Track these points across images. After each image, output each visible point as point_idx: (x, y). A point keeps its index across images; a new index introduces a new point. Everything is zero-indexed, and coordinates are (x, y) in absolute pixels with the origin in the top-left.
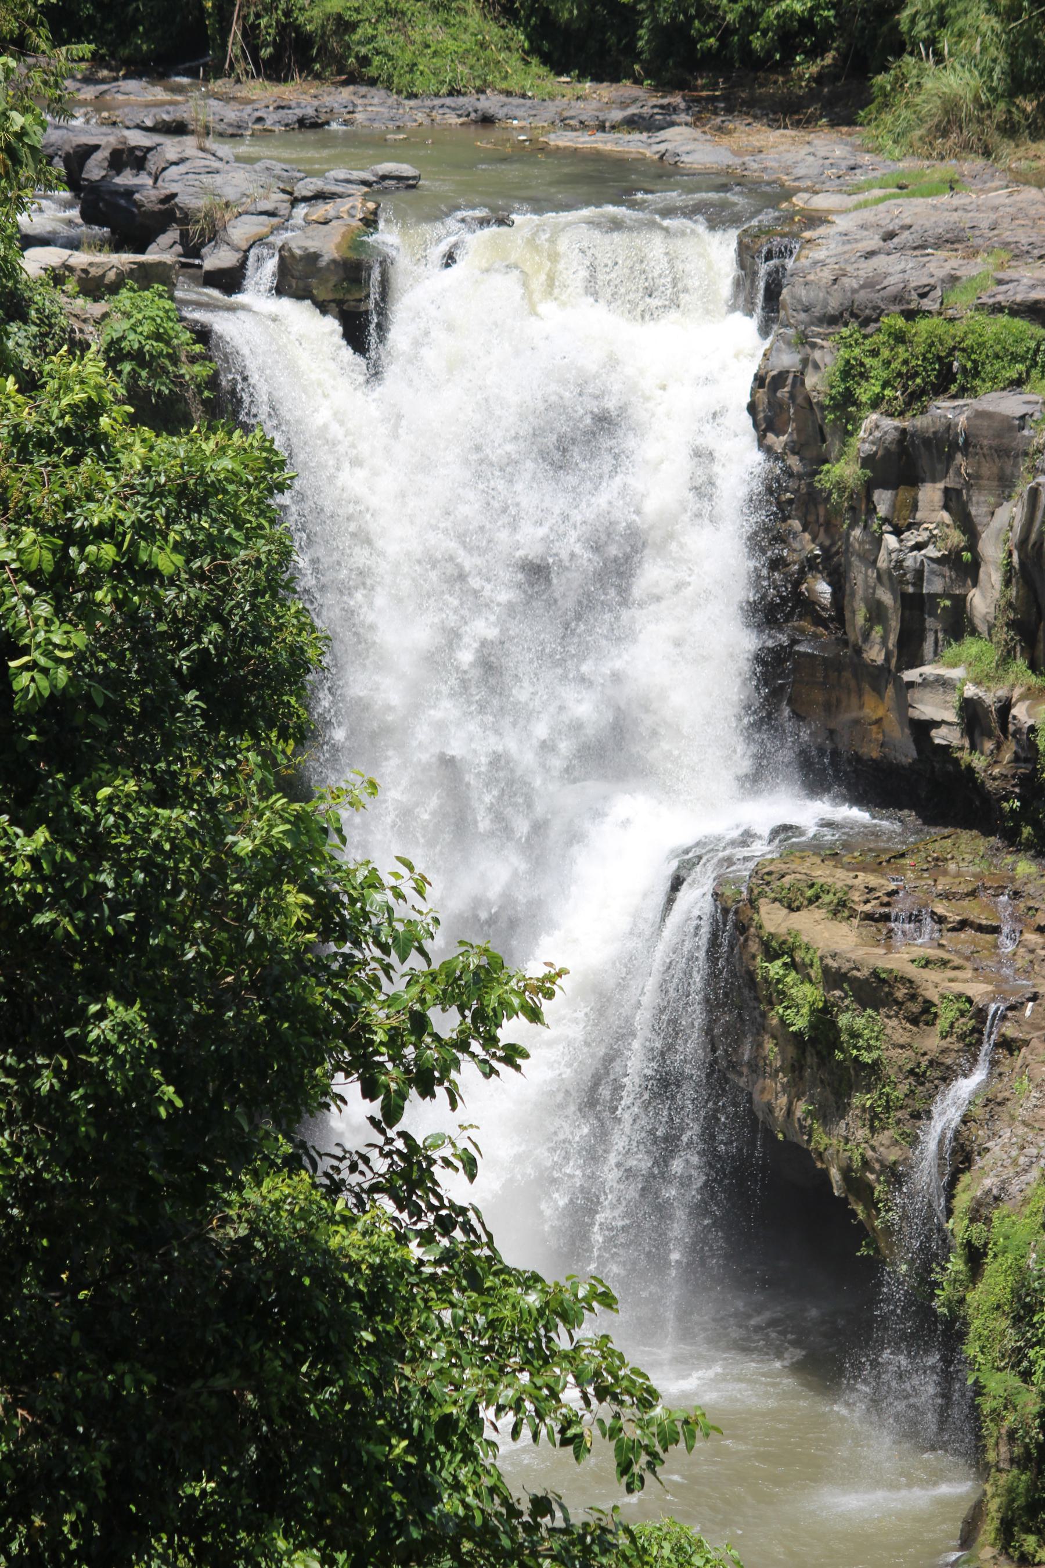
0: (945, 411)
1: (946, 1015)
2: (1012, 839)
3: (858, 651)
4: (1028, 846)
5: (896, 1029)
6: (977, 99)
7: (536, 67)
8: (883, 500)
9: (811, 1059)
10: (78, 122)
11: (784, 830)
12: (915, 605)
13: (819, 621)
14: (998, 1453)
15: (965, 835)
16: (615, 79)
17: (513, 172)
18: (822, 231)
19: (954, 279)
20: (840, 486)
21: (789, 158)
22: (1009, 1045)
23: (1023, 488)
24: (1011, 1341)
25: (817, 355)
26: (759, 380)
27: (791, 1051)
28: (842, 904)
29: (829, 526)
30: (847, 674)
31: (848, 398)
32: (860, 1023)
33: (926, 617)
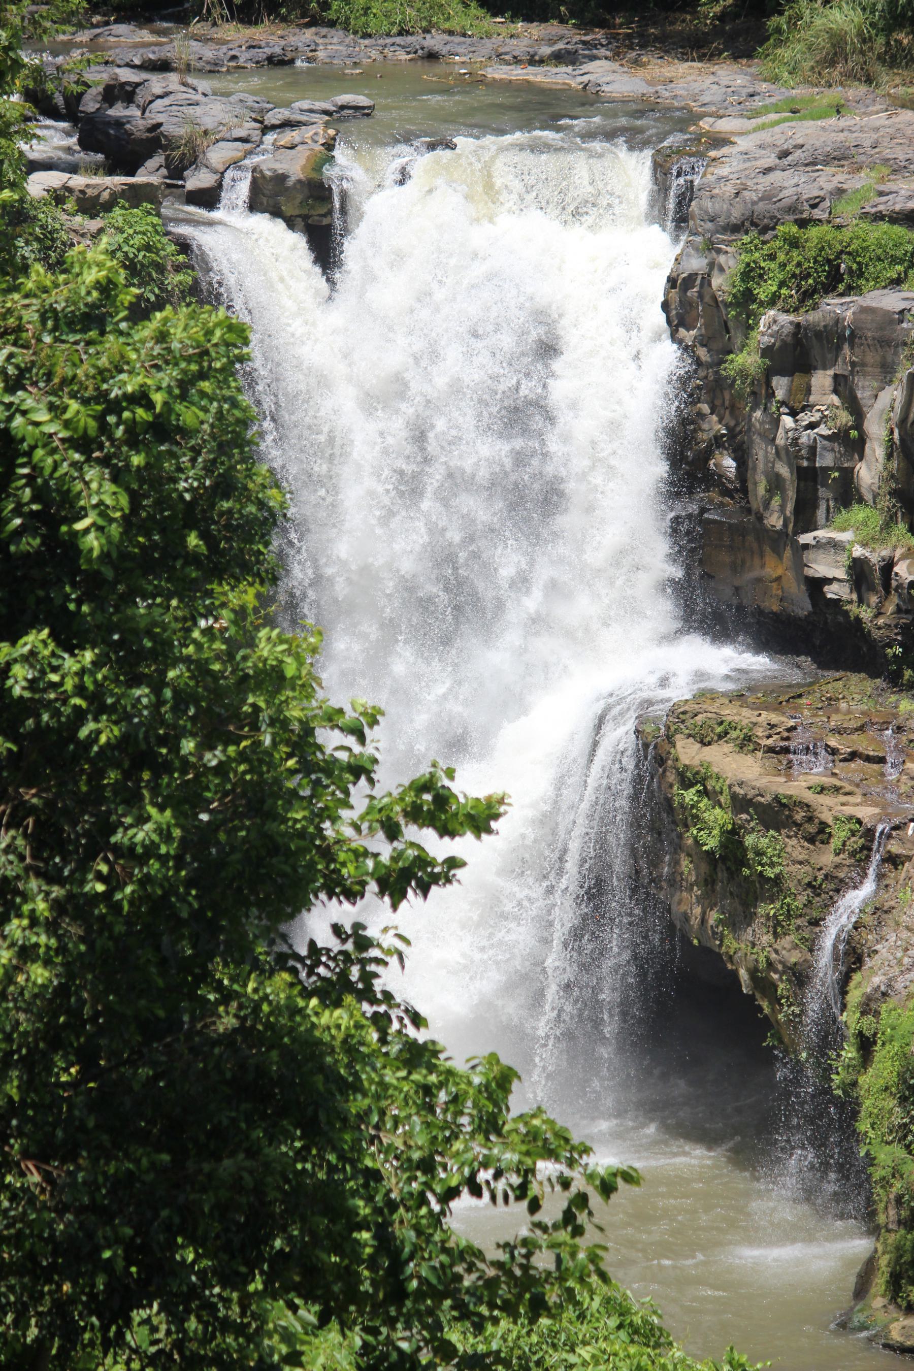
0: (836, 307)
1: (839, 835)
3: (760, 518)
5: (795, 847)
6: (860, 34)
8: (781, 386)
9: (722, 875)
15: (855, 678)
18: (725, 150)
19: (840, 192)
20: (743, 373)
21: (696, 87)
22: (894, 861)
25: (722, 259)
26: (672, 282)
27: (704, 868)
28: (748, 739)
29: (733, 409)
30: (750, 538)
31: (748, 297)
32: (764, 842)
33: (819, 487)
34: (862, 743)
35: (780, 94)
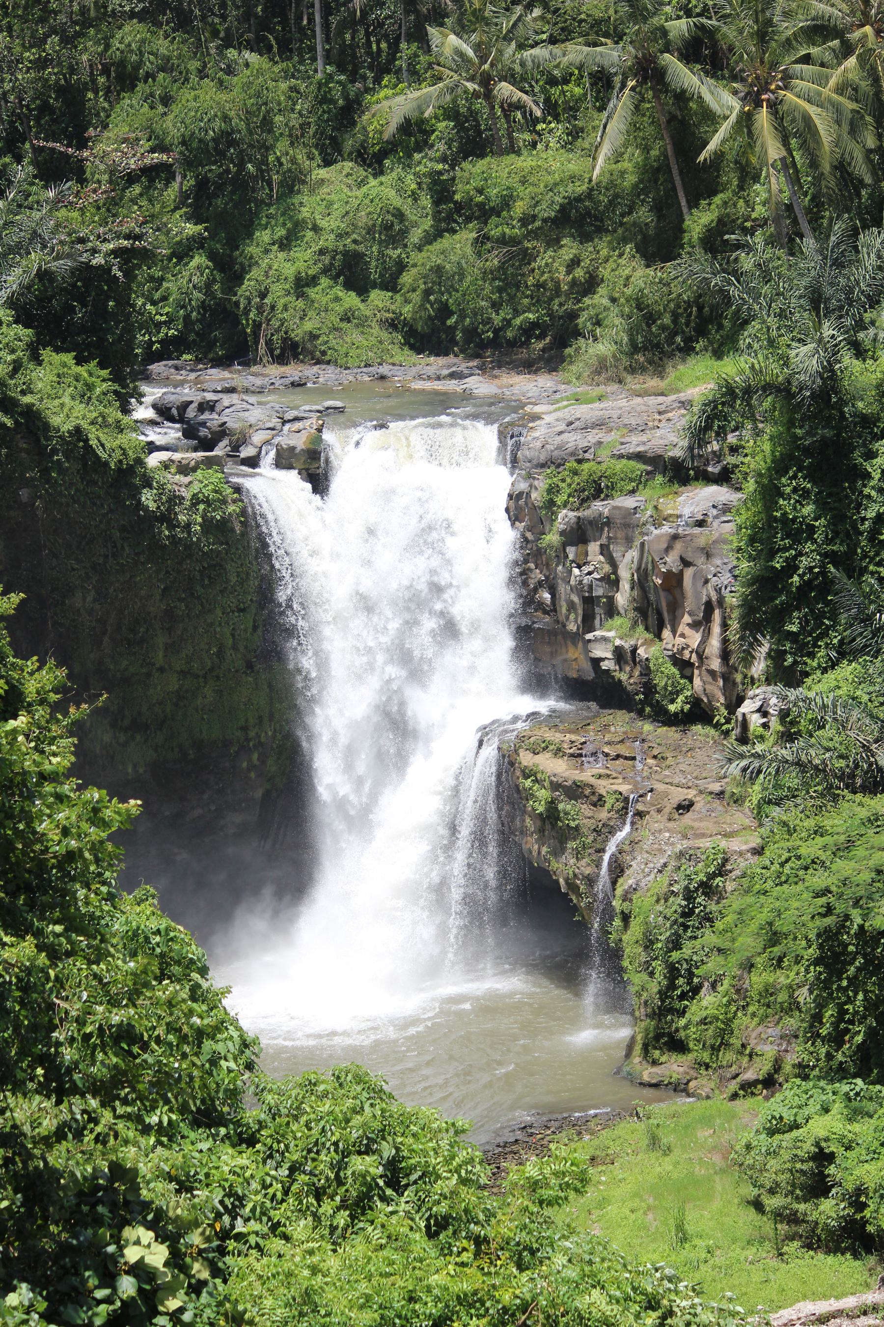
0: (600, 507)
1: (610, 801)
2: (640, 713)
3: (564, 626)
4: (649, 717)
5: (586, 809)
6: (614, 356)
7: (407, 351)
8: (571, 551)
9: (548, 826)
10: (186, 391)
11: (533, 716)
12: (589, 602)
13: (545, 612)
14: (641, 1012)
15: (619, 713)
16: (446, 354)
17: (393, 402)
18: (538, 423)
21: (525, 388)
22: (640, 814)
23: (637, 543)
24: (643, 958)
25: (536, 483)
26: (510, 496)
27: (539, 823)
28: (559, 750)
29: (548, 565)
30: (560, 637)
31: (551, 503)
32: (569, 807)
33: (594, 608)
34: (623, 750)
35: (570, 390)
